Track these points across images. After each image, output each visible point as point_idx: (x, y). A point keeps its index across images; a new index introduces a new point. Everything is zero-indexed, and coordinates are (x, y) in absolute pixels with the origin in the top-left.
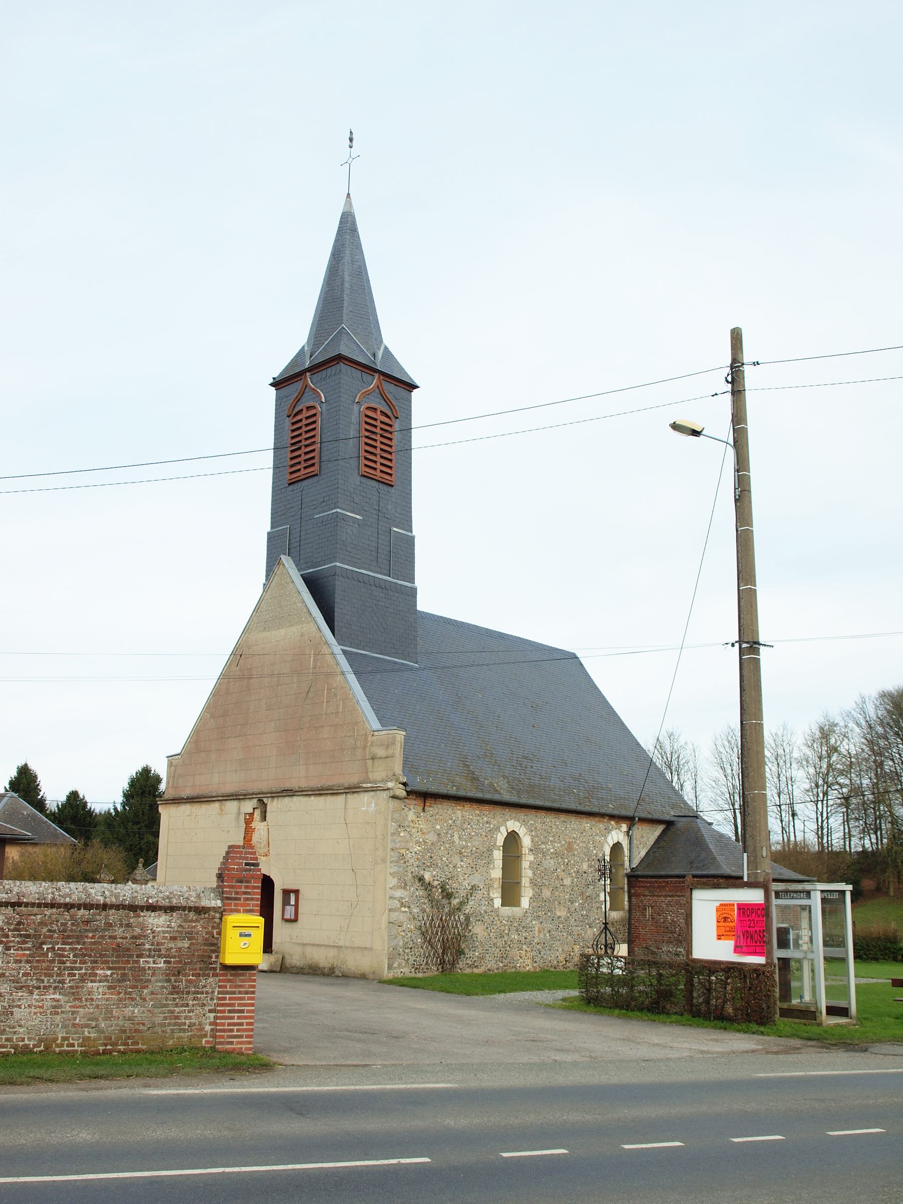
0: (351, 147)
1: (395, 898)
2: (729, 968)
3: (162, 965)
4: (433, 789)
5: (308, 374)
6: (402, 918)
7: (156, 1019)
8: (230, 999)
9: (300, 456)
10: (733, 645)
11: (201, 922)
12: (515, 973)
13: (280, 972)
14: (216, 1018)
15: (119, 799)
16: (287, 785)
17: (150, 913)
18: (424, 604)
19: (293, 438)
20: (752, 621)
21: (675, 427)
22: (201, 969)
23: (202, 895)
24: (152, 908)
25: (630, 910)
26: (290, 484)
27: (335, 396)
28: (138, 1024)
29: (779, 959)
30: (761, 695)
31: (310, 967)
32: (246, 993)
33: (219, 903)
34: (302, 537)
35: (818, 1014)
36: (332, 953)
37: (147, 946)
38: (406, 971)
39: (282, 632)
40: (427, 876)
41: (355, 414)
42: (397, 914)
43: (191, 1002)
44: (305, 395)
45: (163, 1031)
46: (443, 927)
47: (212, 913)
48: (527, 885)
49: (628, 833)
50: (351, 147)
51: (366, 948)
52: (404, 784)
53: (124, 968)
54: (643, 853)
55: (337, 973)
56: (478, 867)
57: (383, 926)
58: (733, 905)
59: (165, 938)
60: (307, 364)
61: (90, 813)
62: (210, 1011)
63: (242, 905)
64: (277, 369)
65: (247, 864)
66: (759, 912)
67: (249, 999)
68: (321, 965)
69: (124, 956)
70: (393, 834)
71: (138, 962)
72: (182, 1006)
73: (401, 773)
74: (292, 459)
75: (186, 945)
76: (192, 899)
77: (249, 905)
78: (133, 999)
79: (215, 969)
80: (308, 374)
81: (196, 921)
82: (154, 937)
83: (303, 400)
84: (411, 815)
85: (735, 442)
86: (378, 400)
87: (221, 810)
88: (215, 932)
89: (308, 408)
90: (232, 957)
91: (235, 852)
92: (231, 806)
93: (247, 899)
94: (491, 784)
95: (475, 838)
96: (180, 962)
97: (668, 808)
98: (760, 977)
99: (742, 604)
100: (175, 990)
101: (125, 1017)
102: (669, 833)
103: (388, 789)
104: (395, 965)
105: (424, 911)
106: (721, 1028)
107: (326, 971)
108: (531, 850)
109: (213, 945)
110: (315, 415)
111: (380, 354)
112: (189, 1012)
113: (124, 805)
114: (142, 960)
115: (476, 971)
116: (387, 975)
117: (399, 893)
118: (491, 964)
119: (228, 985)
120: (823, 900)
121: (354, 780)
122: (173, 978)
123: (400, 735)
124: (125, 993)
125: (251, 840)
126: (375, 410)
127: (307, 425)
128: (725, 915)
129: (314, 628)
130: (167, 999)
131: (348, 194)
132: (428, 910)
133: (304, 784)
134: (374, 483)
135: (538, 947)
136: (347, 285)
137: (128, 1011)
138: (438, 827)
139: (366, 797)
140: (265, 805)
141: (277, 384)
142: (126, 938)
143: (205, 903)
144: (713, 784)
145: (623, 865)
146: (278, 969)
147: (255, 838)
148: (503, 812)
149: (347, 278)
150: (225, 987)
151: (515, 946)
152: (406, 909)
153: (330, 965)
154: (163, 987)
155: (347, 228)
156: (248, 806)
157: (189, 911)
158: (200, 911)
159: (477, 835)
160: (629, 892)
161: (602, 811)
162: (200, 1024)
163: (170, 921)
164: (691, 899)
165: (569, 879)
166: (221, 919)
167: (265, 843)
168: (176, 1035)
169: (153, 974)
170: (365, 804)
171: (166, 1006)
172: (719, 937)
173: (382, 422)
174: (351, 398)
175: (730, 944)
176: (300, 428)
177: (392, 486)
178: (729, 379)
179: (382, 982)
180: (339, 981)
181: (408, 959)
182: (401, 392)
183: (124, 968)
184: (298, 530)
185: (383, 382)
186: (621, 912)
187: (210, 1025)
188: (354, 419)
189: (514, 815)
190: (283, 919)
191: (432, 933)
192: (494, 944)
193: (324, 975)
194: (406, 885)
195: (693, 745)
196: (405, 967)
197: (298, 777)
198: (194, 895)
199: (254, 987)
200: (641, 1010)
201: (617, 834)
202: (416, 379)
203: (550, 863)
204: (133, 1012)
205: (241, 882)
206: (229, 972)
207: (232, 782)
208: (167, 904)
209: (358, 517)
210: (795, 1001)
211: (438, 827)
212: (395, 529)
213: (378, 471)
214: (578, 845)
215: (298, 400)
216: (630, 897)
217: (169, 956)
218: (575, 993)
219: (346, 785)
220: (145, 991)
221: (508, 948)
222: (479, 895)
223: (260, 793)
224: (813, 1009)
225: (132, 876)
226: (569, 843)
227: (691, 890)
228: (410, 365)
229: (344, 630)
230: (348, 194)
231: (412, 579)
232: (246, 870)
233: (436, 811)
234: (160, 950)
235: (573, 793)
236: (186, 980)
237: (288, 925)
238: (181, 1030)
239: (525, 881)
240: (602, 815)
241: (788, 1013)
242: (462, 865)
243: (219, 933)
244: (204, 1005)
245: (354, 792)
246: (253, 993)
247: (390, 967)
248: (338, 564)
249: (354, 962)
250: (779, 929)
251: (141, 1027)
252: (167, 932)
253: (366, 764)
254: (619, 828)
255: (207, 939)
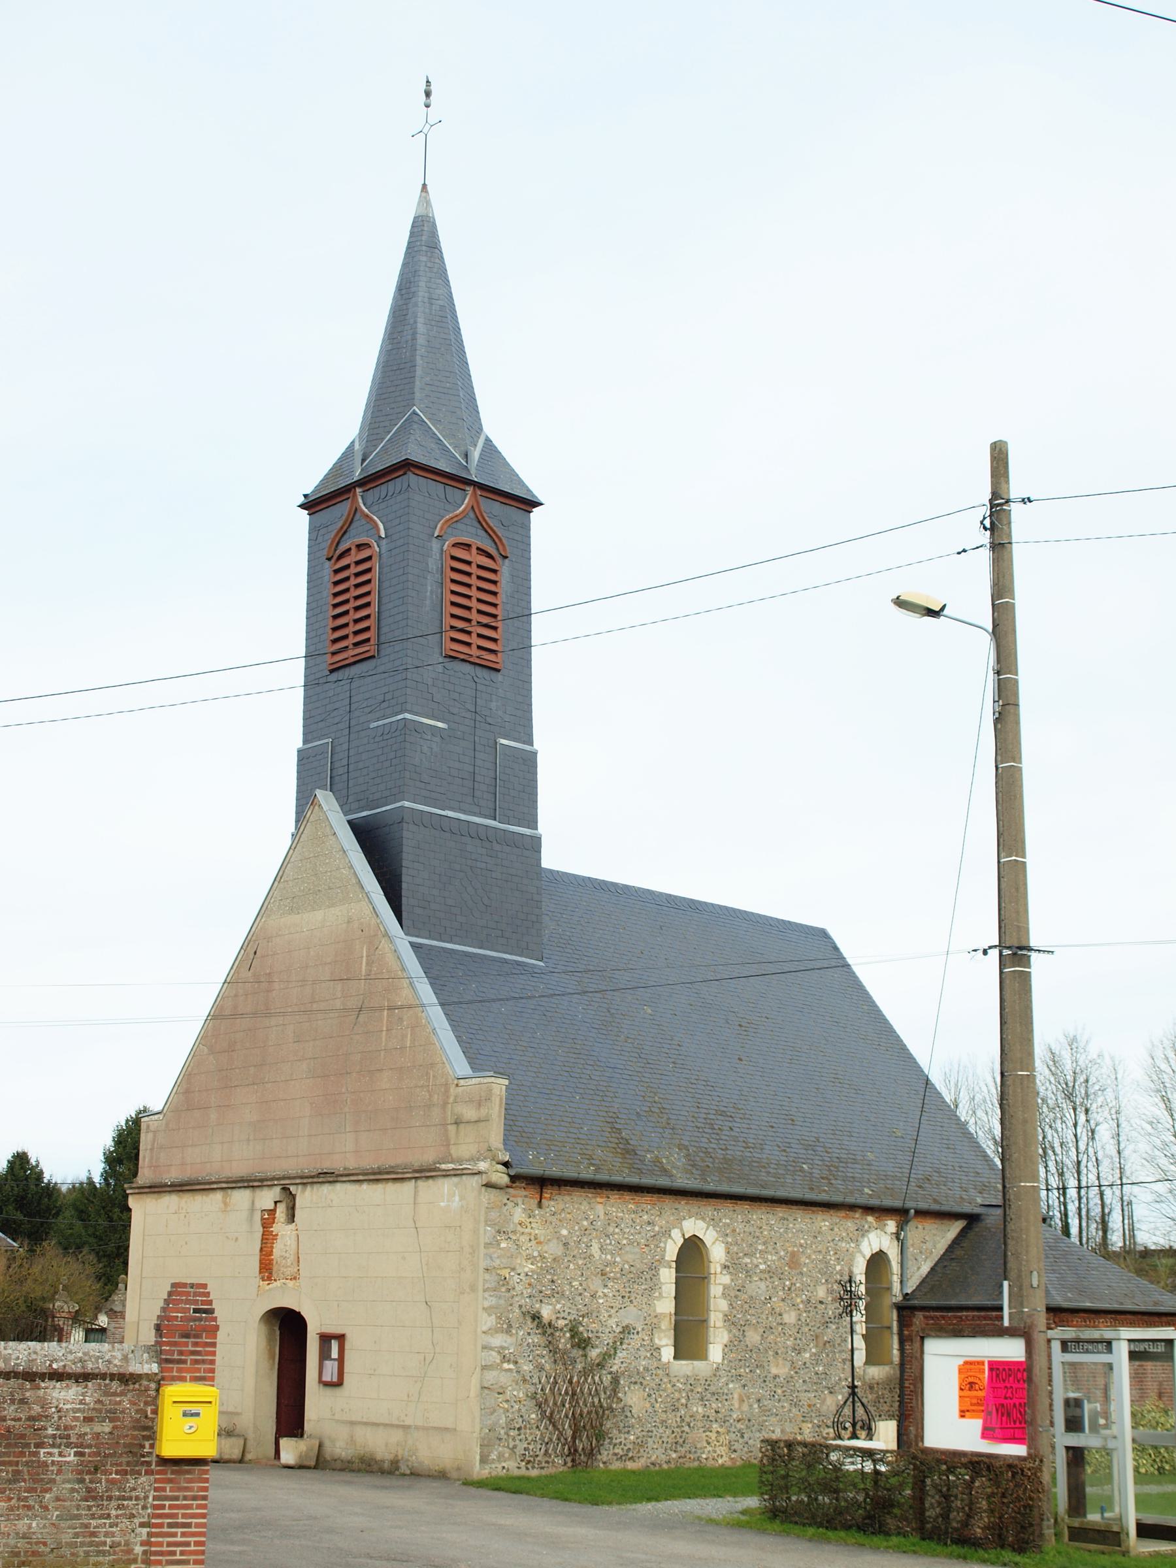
0: (427, 106)
1: (491, 1349)
2: (977, 1464)
3: (71, 1458)
4: (555, 1171)
5: (358, 490)
6: (504, 1379)
7: (63, 1536)
8: (171, 1507)
9: (346, 625)
10: (985, 952)
11: (129, 1395)
12: (699, 1469)
13: (315, 1468)
14: (150, 1535)
15: (103, 1165)
16: (327, 1165)
17: (54, 1383)
18: (550, 860)
19: (336, 595)
20: (1018, 912)
21: (900, 603)
22: (128, 1464)
23: (131, 1356)
24: (57, 1376)
25: (902, 1365)
26: (332, 671)
27: (401, 527)
28: (37, 1543)
29: (1068, 1448)
30: (1032, 1031)
31: (362, 1460)
32: (195, 1498)
33: (155, 1368)
34: (352, 760)
35: (1123, 1536)
36: (396, 1436)
37: (50, 1431)
38: (512, 1466)
39: (319, 915)
40: (546, 1313)
41: (435, 555)
42: (495, 1373)
43: (113, 1512)
44: (354, 525)
45: (72, 1554)
46: (574, 1394)
47: (145, 1383)
48: (720, 1324)
49: (897, 1236)
50: (427, 106)
51: (446, 1429)
52: (506, 1164)
53: (17, 1464)
54: (925, 1269)
55: (404, 1469)
56: (633, 1296)
57: (473, 1394)
58: (983, 1363)
59: (76, 1419)
60: (357, 475)
61: (51, 1191)
62: (142, 1525)
63: (188, 1371)
64: (310, 481)
65: (195, 1311)
66: (1019, 1375)
67: (199, 1507)
68: (378, 1458)
69: (16, 1445)
70: (487, 1245)
71: (36, 1454)
72: (101, 1517)
73: (501, 1146)
74: (334, 629)
75: (107, 1430)
76: (116, 1362)
77: (199, 1370)
78: (29, 1508)
79: (149, 1463)
80: (358, 490)
81: (122, 1394)
82: (60, 1418)
83: (353, 531)
84: (519, 1214)
85: (995, 626)
86: (473, 530)
87: (225, 1204)
88: (149, 1409)
89: (360, 547)
90: (170, 1447)
91: (180, 1294)
92: (241, 1197)
93: (196, 1362)
94: (657, 1161)
95: (628, 1248)
96: (98, 1454)
97: (972, 1192)
98: (1018, 1477)
99: (1003, 886)
100: (91, 1495)
101: (17, 1534)
102: (971, 1235)
103: (479, 1173)
104: (493, 1456)
105: (541, 1368)
106: (959, 1557)
107: (386, 1465)
108: (725, 1267)
109: (146, 1428)
110: (369, 558)
111: (476, 454)
112: (111, 1527)
113: (106, 1176)
114: (42, 1451)
115: (630, 1465)
116: (479, 1471)
117: (498, 1340)
118: (656, 1454)
119: (168, 1486)
120: (1133, 1355)
121: (427, 1157)
122: (87, 1477)
123: (500, 1085)
124: (19, 1499)
125: (271, 1253)
126: (468, 546)
127: (357, 575)
128: (971, 1380)
129: (367, 911)
130: (78, 1507)
131: (424, 186)
132: (547, 1367)
133: (352, 1163)
134: (467, 668)
135: (739, 1426)
136: (421, 340)
137: (22, 1525)
138: (564, 1232)
139: (446, 1185)
140: (293, 1197)
141: (312, 505)
142: (20, 1419)
143: (135, 1368)
144: (1148, 1127)
145: (889, 1289)
146: (313, 1463)
147: (278, 1250)
148: (677, 1205)
149: (421, 328)
150: (164, 1489)
151: (700, 1424)
152: (511, 1366)
153: (391, 1457)
154: (73, 1490)
155: (423, 243)
156: (267, 1198)
157: (111, 1380)
158: (126, 1379)
159: (631, 1243)
160: (900, 1334)
161: (850, 1200)
162: (127, 1544)
163: (83, 1394)
164: (922, 1352)
165: (793, 1314)
166: (157, 1390)
167: (291, 1258)
168: (92, 1559)
169: (59, 1472)
170: (446, 1197)
171: (78, 1517)
172: (963, 1414)
173: (479, 567)
174: (418, 539)
175: (975, 1425)
176: (347, 579)
177: (498, 671)
178: (987, 523)
179: (467, 1483)
180: (406, 1482)
181: (515, 1447)
182: (512, 513)
183: (17, 1464)
184: (345, 746)
185: (481, 500)
186: (887, 1368)
187: (142, 1545)
188: (433, 563)
189: (695, 1209)
190: (320, 1381)
191: (555, 1404)
192: (663, 1422)
193: (383, 1473)
194: (510, 1326)
195: (1112, 1058)
196: (509, 1459)
197: (345, 1152)
198: (120, 1357)
199: (205, 1489)
200: (847, 1527)
201: (879, 1238)
202: (538, 491)
203: (759, 1288)
204: (30, 1527)
205: (187, 1336)
206: (170, 1469)
207: (241, 1158)
208: (79, 1370)
209: (440, 725)
210: (1093, 1517)
211: (564, 1232)
212: (503, 741)
213: (474, 647)
214: (809, 1257)
215: (343, 532)
216: (902, 1342)
217: (81, 1446)
218: (752, 1502)
219: (416, 1166)
220: (48, 1496)
221: (686, 1429)
222: (634, 1341)
223: (284, 1178)
224: (1115, 1529)
225: (108, 1305)
226: (793, 1254)
227: (922, 1338)
228: (528, 464)
229: (418, 911)
230: (424, 186)
231: (533, 823)
232: (195, 1319)
233: (561, 1206)
234: (68, 1437)
235: (802, 1170)
236: (107, 1481)
237: (329, 1391)
238: (99, 1553)
239: (715, 1319)
240: (852, 1207)
241: (1080, 1534)
242: (605, 1294)
243: (155, 1412)
244: (133, 1516)
245: (428, 1177)
246: (205, 1498)
247: (484, 1460)
248: (407, 804)
249: (430, 1452)
250: (1067, 1402)
251: (42, 1548)
252: (79, 1410)
253: (446, 1130)
254: (882, 1228)
255: (138, 1421)
